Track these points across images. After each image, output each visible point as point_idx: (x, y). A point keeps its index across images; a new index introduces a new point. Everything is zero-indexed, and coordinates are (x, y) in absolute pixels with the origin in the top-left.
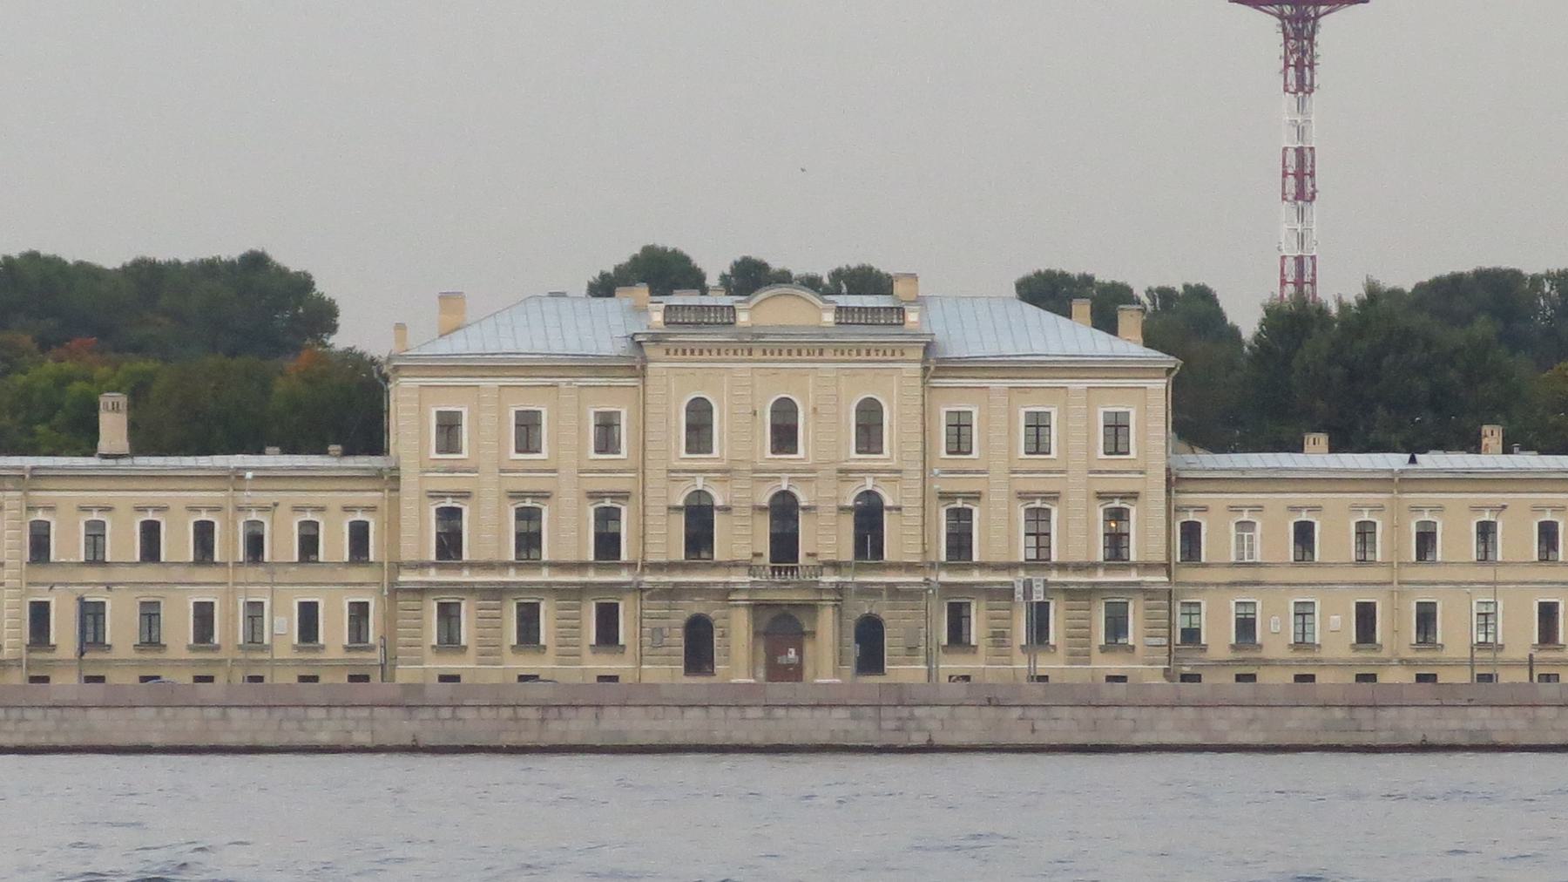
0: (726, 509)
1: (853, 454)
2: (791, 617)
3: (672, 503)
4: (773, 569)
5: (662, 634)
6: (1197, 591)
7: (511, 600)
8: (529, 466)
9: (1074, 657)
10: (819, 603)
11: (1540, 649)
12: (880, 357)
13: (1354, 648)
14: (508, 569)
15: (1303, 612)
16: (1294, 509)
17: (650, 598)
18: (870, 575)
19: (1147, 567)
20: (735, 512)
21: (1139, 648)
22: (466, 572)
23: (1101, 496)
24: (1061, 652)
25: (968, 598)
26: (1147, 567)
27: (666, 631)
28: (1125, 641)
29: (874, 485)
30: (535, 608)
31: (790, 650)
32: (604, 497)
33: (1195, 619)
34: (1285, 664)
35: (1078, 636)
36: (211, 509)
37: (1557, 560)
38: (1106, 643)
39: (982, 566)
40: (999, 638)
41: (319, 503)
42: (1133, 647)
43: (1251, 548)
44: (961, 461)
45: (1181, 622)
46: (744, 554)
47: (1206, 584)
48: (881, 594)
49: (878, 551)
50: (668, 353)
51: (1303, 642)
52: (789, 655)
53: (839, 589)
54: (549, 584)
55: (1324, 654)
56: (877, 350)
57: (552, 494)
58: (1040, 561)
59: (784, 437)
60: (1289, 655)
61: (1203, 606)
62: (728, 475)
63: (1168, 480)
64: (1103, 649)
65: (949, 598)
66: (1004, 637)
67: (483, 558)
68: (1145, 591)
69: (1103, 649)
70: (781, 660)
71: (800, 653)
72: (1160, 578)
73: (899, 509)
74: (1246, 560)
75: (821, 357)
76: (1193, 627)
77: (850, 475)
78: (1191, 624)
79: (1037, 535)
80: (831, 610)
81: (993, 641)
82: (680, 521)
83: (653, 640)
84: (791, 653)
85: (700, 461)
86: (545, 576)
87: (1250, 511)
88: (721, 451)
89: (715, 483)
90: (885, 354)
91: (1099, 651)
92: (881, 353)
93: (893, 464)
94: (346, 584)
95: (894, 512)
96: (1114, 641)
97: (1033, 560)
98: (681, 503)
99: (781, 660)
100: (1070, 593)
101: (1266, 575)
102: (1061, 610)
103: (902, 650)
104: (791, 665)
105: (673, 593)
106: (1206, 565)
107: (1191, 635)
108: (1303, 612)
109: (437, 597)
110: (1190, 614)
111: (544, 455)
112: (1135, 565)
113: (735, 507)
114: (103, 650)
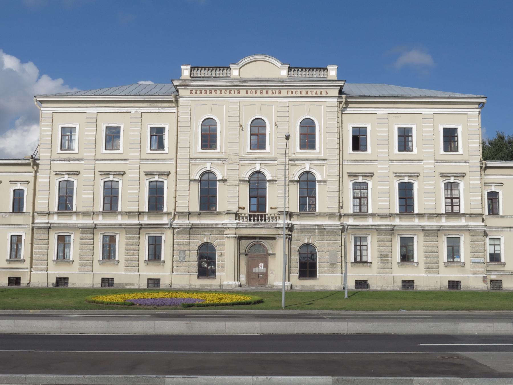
0: (224, 181)
2: (261, 245)
3: (192, 178)
5: (185, 254)
6: (497, 232)
7: (443, 236)
8: (112, 157)
10: (277, 236)
12: (314, 95)
13: (9, 262)
17: (178, 233)
19: (472, 216)
20: (328, 183)
21: (468, 266)
22: (119, 217)
23: (443, 175)
24: (76, 264)
26: (472, 216)
27: (187, 253)
28: (459, 260)
29: (310, 168)
30: (113, 239)
31: (261, 264)
32: (404, 176)
33: (497, 248)
36: (22, 182)
38: (448, 261)
39: (421, 216)
40: (384, 258)
42: (464, 264)
44: (359, 155)
45: (490, 250)
46: (234, 208)
48: (314, 232)
49: (313, 205)
51: (361, 261)
52: (260, 268)
53: (291, 228)
54: (120, 224)
56: (312, 91)
57: (374, 174)
58: (362, 213)
61: (502, 240)
62: (326, 162)
64: (447, 265)
65: (355, 234)
66: (387, 257)
67: (128, 210)
69: (447, 265)
70: (255, 270)
71: (266, 266)
73: (325, 181)
76: (496, 252)
77: (296, 162)
78: (494, 251)
79: (360, 198)
81: (381, 259)
82: (196, 189)
83: (179, 258)
84: (261, 266)
85: (209, 153)
86: (119, 220)
88: (221, 148)
91: (444, 266)
93: (322, 156)
95: (322, 183)
96: (452, 260)
97: (358, 212)
98: (197, 178)
99: (255, 270)
100: (426, 231)
102: (422, 243)
103: (327, 264)
104: (262, 273)
105: (191, 229)
106: (503, 217)
107: (495, 258)
110: (494, 245)
111: (121, 151)
112: (464, 215)
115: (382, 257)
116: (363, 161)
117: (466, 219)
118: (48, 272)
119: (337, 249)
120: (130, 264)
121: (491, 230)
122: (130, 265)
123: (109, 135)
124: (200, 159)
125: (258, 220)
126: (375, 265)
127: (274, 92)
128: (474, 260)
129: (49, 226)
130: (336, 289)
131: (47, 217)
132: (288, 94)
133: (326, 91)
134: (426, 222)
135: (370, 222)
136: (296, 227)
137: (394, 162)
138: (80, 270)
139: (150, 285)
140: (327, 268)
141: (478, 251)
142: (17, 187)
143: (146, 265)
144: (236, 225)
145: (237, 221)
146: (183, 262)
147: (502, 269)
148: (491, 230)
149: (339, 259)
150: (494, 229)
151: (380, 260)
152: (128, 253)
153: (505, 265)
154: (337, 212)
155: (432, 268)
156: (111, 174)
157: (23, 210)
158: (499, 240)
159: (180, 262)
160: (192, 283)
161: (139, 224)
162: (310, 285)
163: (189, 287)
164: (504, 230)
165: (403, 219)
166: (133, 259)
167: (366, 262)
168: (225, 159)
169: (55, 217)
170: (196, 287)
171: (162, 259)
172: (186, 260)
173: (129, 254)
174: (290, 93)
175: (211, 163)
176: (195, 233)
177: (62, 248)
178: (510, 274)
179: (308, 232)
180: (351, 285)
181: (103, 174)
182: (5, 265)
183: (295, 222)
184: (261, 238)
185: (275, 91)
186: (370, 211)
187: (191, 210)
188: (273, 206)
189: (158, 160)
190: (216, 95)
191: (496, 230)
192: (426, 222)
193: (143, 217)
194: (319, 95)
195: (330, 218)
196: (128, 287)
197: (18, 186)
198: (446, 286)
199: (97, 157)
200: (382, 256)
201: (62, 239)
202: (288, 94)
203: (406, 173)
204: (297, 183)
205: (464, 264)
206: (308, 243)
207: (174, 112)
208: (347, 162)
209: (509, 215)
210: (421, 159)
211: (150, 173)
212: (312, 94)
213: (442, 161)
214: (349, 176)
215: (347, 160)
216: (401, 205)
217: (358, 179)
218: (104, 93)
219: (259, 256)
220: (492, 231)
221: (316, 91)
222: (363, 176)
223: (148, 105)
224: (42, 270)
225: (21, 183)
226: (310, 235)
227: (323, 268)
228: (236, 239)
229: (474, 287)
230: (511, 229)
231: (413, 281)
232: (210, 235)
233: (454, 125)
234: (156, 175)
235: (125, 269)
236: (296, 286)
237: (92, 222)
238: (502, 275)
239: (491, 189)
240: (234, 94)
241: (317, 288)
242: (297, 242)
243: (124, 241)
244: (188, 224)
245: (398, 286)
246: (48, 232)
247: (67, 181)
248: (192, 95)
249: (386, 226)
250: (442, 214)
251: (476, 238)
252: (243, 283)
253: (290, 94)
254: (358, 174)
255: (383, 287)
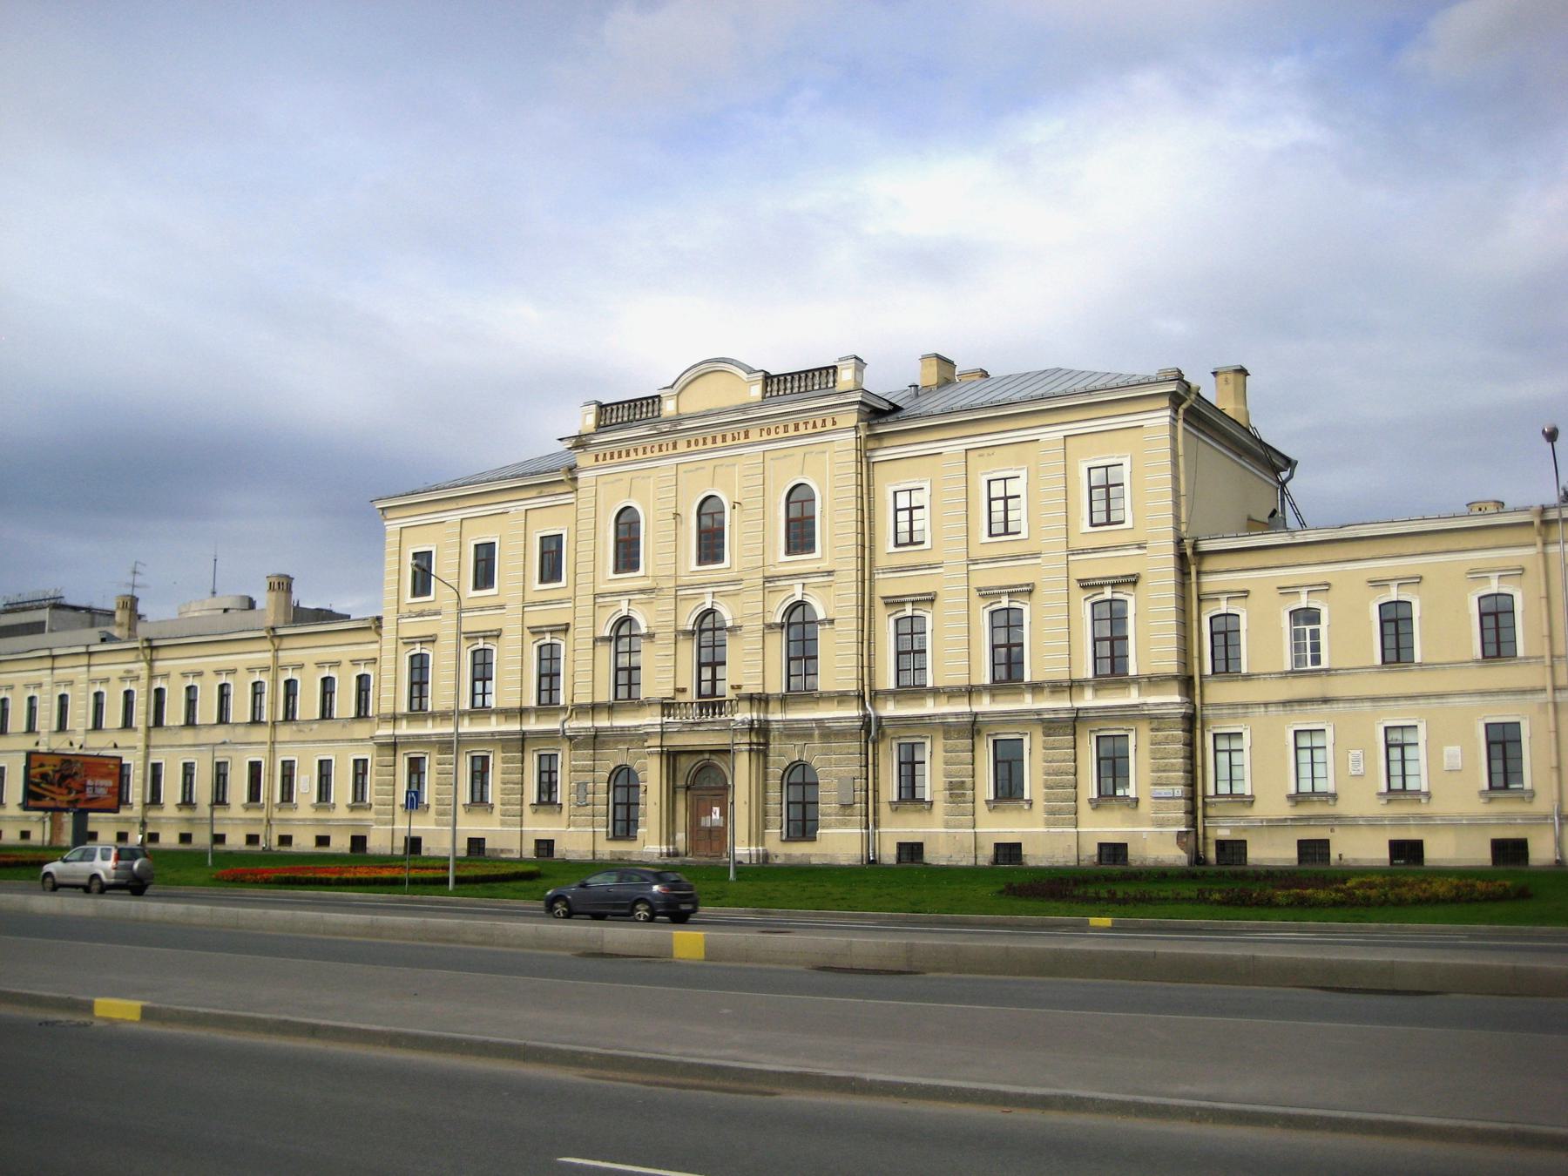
0: (650, 636)
1: (783, 557)
3: (599, 634)
4: (701, 706)
6: (1234, 717)
9: (1064, 811)
11: (1389, 801)
12: (811, 430)
14: (426, 720)
15: (1396, 744)
16: (1378, 583)
18: (801, 710)
20: (837, 626)
21: (1145, 806)
22: (930, 702)
25: (920, 737)
31: (714, 808)
34: (1373, 823)
35: (1063, 785)
36: (1403, 582)
37: (1413, 662)
40: (958, 791)
41: (298, 661)
42: (1137, 800)
43: (1316, 647)
46: (667, 691)
47: (1246, 705)
48: (811, 736)
50: (597, 460)
52: (714, 816)
55: (1436, 808)
56: (806, 423)
59: (711, 545)
60: (1378, 808)
63: (1181, 557)
64: (1096, 804)
65: (900, 738)
66: (963, 789)
68: (1152, 718)
69: (1096, 804)
70: (705, 822)
72: (853, 711)
73: (832, 622)
74: (1310, 667)
75: (675, 452)
77: (778, 583)
80: (746, 755)
81: (951, 794)
84: (715, 813)
87: (1399, 584)
89: (817, 590)
90: (814, 426)
92: (810, 426)
93: (825, 566)
94: (181, 746)
99: (705, 822)
101: (1336, 687)
105: (596, 740)
108: (1396, 744)
109: (406, 752)
112: (1136, 680)
113: (659, 633)
114: (291, 809)
115: (952, 790)
116: (915, 568)
117: (1139, 690)
118: (524, 829)
119: (854, 771)
120: (507, 810)
121: (1219, 712)
122: (508, 813)
123: (625, 541)
124: (612, 594)
125: (714, 713)
126: (940, 808)
127: (736, 435)
128: (1157, 791)
129: (393, 741)
130: (851, 863)
131: (966, 700)
132: (761, 436)
133: (833, 419)
134: (1046, 703)
135: (929, 707)
136: (775, 726)
137: (977, 564)
138: (1048, 824)
139: (541, 852)
140: (836, 815)
141: (1167, 768)
142: (1390, 596)
143: (1093, 809)
144: (659, 727)
145: (665, 719)
146: (583, 806)
147: (1247, 812)
148: (1219, 712)
149: (860, 795)
150: (1225, 711)
151: (948, 796)
152: (505, 789)
153: (1253, 801)
154: (855, 689)
155: (1060, 811)
156: (1107, 585)
157: (66, 727)
158: (1414, 729)
159: (579, 806)
160: (599, 848)
161: (1072, 709)
162: (803, 854)
163: (591, 857)
164: (1250, 710)
165: (542, 718)
166: (513, 801)
167: (922, 801)
168: (652, 590)
169: (986, 699)
170: (605, 858)
171: (1026, 796)
172: (588, 802)
173: (507, 792)
174: (764, 433)
175: (630, 600)
176: (604, 744)
177: (415, 780)
178: (1265, 824)
179: (798, 736)
180: (889, 854)
181: (986, 593)
182: (1479, 807)
183: (776, 715)
184: (712, 752)
185: (739, 433)
186: (929, 684)
187: (598, 700)
188: (735, 684)
189: (550, 602)
190: (638, 457)
191: (1230, 711)
192: (1046, 703)
193: (886, 703)
194: (819, 429)
195: (839, 702)
196: (503, 856)
197: (1393, 594)
198: (1093, 856)
199: (973, 555)
200: (952, 786)
201: (416, 766)
202: (761, 436)
203: (1001, 588)
204: (780, 630)
205: (1137, 800)
206: (800, 760)
207: (573, 503)
208: (883, 573)
209: (1263, 671)
210: (1035, 549)
211: (926, 597)
212: (806, 429)
213: (1083, 550)
214: (886, 604)
215: (882, 569)
216: (1018, 663)
217: (904, 610)
218: (1074, 387)
219: (712, 793)
220: (1220, 717)
221: (814, 422)
222: (913, 602)
223: (534, 493)
224: (386, 824)
225: (1308, 592)
226: (804, 742)
227: (829, 815)
228: (664, 757)
229: (1156, 860)
230: (1270, 709)
231: (1019, 845)
232: (628, 749)
233: (1113, 457)
234: (547, 631)
235: (501, 820)
236: (776, 856)
237: (1067, 704)
238: (1245, 829)
239: (1220, 609)
240: (667, 450)
241: (814, 861)
242: (780, 760)
243: (1039, 751)
244: (589, 728)
245: (986, 856)
246: (393, 753)
247: (1008, 609)
248: (598, 463)
249: (957, 715)
250: (1086, 680)
251: (1163, 735)
252: (681, 847)
253: (765, 437)
254: (903, 599)
255: (953, 859)
